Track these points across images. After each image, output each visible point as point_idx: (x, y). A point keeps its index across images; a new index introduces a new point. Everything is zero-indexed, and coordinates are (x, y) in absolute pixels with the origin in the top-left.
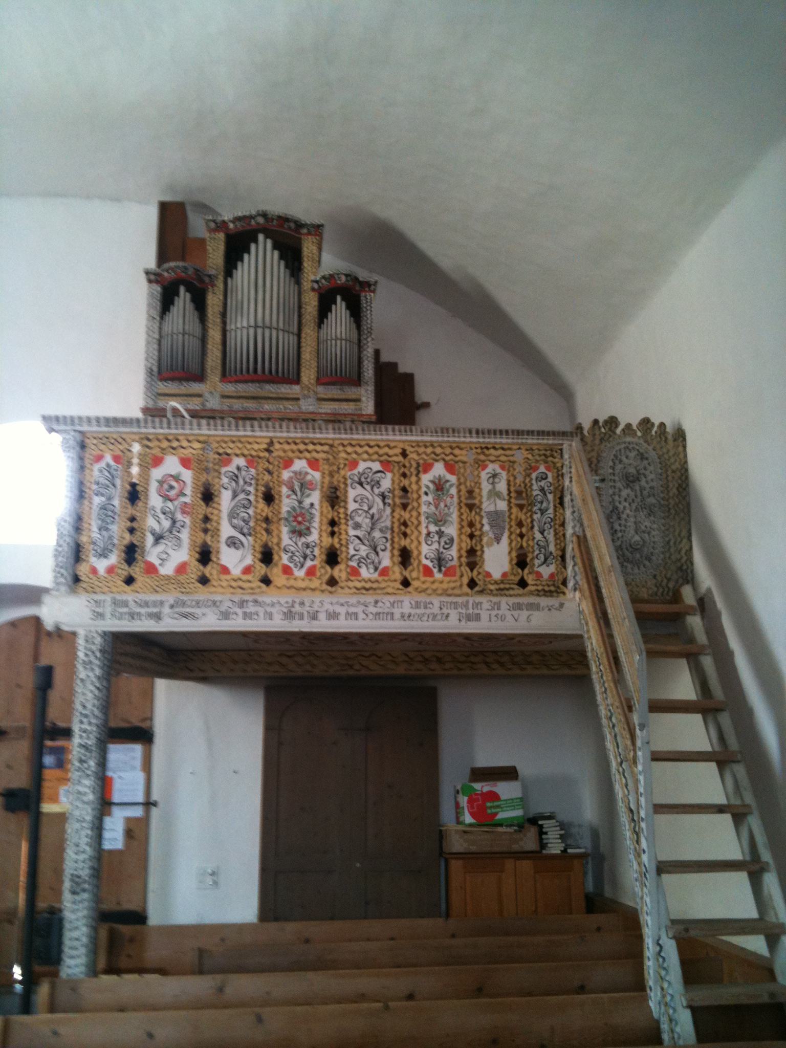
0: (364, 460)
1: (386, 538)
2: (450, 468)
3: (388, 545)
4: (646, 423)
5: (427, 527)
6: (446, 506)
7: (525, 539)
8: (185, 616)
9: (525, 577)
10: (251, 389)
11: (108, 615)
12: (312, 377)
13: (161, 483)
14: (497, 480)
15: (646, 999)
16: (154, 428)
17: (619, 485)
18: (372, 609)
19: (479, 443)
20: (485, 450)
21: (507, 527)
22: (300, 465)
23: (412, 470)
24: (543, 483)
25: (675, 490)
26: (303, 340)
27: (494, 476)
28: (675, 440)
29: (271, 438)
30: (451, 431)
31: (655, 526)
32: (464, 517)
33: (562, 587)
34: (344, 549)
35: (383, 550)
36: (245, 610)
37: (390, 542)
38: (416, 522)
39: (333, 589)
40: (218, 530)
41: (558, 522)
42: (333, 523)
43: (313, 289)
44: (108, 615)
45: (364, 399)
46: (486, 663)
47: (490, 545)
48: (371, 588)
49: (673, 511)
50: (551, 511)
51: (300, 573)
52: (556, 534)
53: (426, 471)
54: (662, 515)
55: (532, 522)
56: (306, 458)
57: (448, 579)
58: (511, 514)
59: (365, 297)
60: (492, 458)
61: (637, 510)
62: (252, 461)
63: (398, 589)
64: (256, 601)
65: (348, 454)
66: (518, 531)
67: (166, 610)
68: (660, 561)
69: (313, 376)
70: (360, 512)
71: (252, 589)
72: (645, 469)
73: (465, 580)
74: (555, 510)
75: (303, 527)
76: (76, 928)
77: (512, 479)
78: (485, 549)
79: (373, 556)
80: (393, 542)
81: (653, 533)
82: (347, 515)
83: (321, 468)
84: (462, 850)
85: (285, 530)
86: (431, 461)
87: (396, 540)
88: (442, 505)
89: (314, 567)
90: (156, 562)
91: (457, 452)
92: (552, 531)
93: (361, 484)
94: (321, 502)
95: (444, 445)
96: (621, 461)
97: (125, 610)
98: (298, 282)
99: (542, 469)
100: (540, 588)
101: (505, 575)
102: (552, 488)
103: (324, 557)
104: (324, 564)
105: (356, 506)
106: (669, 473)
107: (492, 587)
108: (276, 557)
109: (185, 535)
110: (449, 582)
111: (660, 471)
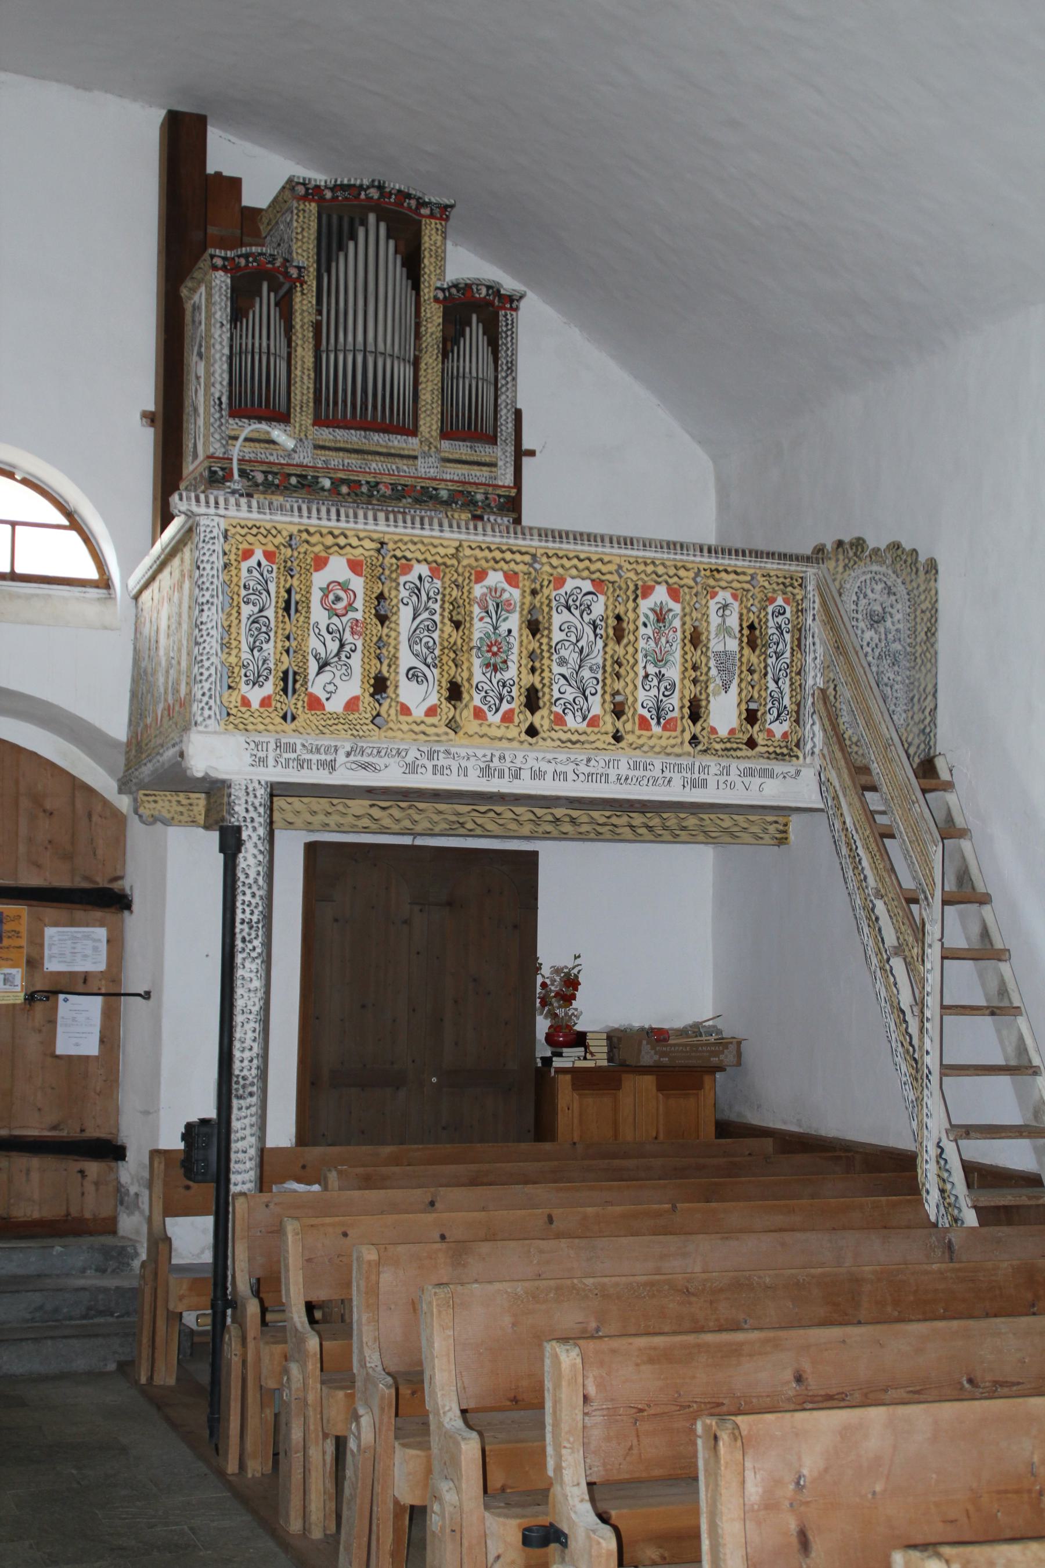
0: (573, 578)
1: (596, 679)
2: (674, 593)
3: (599, 688)
4: (896, 546)
5: (645, 667)
6: (668, 642)
7: (757, 688)
8: (365, 766)
9: (755, 736)
10: (354, 438)
11: (271, 762)
12: (434, 427)
13: (326, 591)
14: (727, 612)
15: (920, 1203)
16: (319, 519)
17: (862, 625)
18: (583, 768)
19: (710, 563)
20: (715, 573)
21: (737, 672)
22: (495, 578)
23: (629, 593)
24: (780, 619)
25: (923, 634)
26: (422, 373)
27: (725, 607)
28: (927, 572)
29: (461, 541)
30: (678, 547)
31: (899, 678)
32: (688, 657)
33: (795, 749)
34: (546, 690)
35: (592, 695)
36: (435, 762)
37: (601, 684)
38: (632, 661)
39: (533, 740)
40: (397, 658)
41: (794, 669)
42: (532, 656)
43: (436, 300)
44: (271, 762)
45: (500, 463)
46: (631, 826)
47: (716, 694)
48: (578, 741)
49: (919, 661)
50: (787, 654)
51: (495, 719)
52: (792, 684)
53: (645, 596)
54: (908, 665)
55: (765, 667)
56: (502, 570)
57: (667, 734)
58: (742, 655)
59: (505, 316)
60: (723, 584)
61: (880, 657)
62: (437, 569)
63: (609, 744)
64: (447, 752)
65: (555, 568)
66: (749, 678)
67: (341, 758)
68: (902, 721)
69: (436, 426)
70: (567, 644)
71: (437, 735)
72: (892, 606)
73: (687, 736)
74: (792, 655)
75: (499, 660)
76: (243, 1138)
77: (745, 611)
78: (711, 698)
79: (580, 700)
80: (605, 684)
81: (896, 687)
82: (551, 647)
83: (521, 585)
84: (651, 1064)
85: (477, 662)
86: (653, 583)
87: (608, 681)
88: (663, 640)
89: (511, 711)
90: (323, 696)
91: (682, 573)
92: (787, 679)
93: (569, 609)
94: (521, 629)
95: (667, 563)
96: (865, 596)
97: (293, 756)
98: (416, 287)
99: (780, 601)
100: (771, 749)
101: (732, 731)
102: (790, 626)
103: (523, 699)
104: (522, 708)
105: (562, 636)
106: (918, 612)
107: (718, 746)
108: (466, 696)
109: (356, 661)
110: (668, 738)
111: (908, 610)
